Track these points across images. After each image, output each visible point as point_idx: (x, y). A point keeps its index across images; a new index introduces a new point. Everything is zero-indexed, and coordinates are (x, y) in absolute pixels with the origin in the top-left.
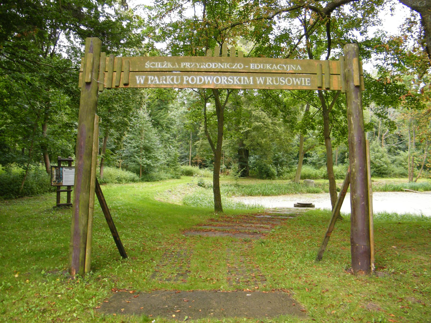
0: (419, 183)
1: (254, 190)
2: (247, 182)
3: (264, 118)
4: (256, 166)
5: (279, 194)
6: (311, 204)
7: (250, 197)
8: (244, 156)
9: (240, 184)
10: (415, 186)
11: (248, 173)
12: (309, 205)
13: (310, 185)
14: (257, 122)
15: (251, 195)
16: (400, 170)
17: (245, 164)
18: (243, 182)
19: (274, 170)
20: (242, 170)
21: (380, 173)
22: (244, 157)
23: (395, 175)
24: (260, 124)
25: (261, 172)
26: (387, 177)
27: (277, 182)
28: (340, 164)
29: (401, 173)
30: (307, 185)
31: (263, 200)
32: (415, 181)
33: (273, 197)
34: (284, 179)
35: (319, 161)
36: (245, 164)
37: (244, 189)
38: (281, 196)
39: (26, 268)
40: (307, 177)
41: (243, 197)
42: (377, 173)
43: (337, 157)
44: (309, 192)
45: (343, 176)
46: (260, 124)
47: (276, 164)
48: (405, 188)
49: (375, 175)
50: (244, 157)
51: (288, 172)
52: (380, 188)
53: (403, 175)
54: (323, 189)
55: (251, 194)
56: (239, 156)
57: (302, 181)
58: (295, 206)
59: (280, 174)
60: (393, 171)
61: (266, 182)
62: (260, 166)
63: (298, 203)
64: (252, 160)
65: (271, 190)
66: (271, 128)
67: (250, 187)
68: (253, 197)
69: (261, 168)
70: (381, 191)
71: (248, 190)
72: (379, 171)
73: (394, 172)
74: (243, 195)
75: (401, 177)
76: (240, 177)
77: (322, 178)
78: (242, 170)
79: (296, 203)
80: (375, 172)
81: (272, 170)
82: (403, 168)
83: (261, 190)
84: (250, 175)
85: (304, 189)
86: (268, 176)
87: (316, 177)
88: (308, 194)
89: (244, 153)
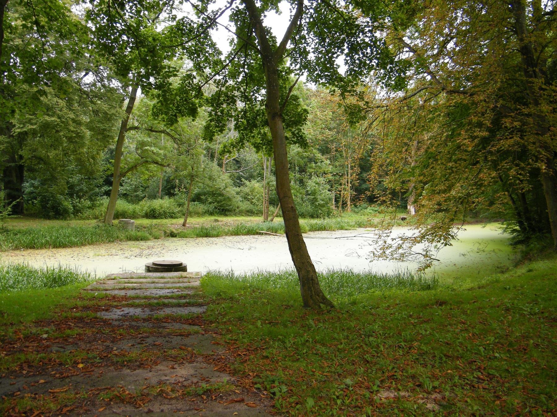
0: (277, 223)
1: (38, 238)
2: (22, 224)
3: (61, 111)
4: (35, 198)
5: (83, 245)
6: (181, 264)
7: (30, 251)
8: (14, 179)
9: (10, 228)
10: (273, 228)
11: (22, 209)
12: (179, 267)
13: (130, 228)
14: (48, 115)
15: (33, 248)
16: (245, 206)
17: (16, 193)
18: (15, 224)
19: (68, 204)
20: (14, 203)
21: (223, 210)
22: (15, 181)
23: (241, 213)
24: (53, 119)
25: (44, 207)
26: (231, 215)
27: (75, 223)
28: (167, 197)
29: (248, 209)
30: (124, 227)
31: (58, 255)
32: (272, 220)
33: (74, 249)
34: (84, 219)
35: (136, 191)
36: (16, 193)
37: (18, 236)
38: (87, 247)
39: (327, 55)
40: (121, 215)
41: (17, 252)
42: (219, 209)
43: (161, 186)
44: (130, 238)
45: (173, 213)
46: (53, 119)
47: (71, 195)
48: (262, 230)
49: (216, 212)
50: (15, 181)
51: (89, 208)
52: (229, 231)
53: (250, 213)
54: (150, 234)
55: (32, 246)
56: (6, 179)
57: (116, 222)
58: (149, 269)
59: (77, 212)
60: (238, 207)
61: (56, 224)
62: (45, 197)
63: (154, 264)
64: (27, 187)
65: (68, 237)
66: (72, 129)
67: (25, 233)
68: (37, 251)
69: (44, 201)
70: (232, 235)
71: (26, 239)
72: (221, 206)
73: (240, 209)
74: (17, 248)
75: (248, 215)
76: (9, 215)
77: (143, 217)
78: (14, 203)
79: (150, 261)
80: (216, 208)
81: (66, 203)
82: (249, 203)
83: (51, 238)
84: (25, 212)
85: (122, 235)
86: (56, 212)
87: (134, 216)
88: (130, 243)
89: (14, 174)
